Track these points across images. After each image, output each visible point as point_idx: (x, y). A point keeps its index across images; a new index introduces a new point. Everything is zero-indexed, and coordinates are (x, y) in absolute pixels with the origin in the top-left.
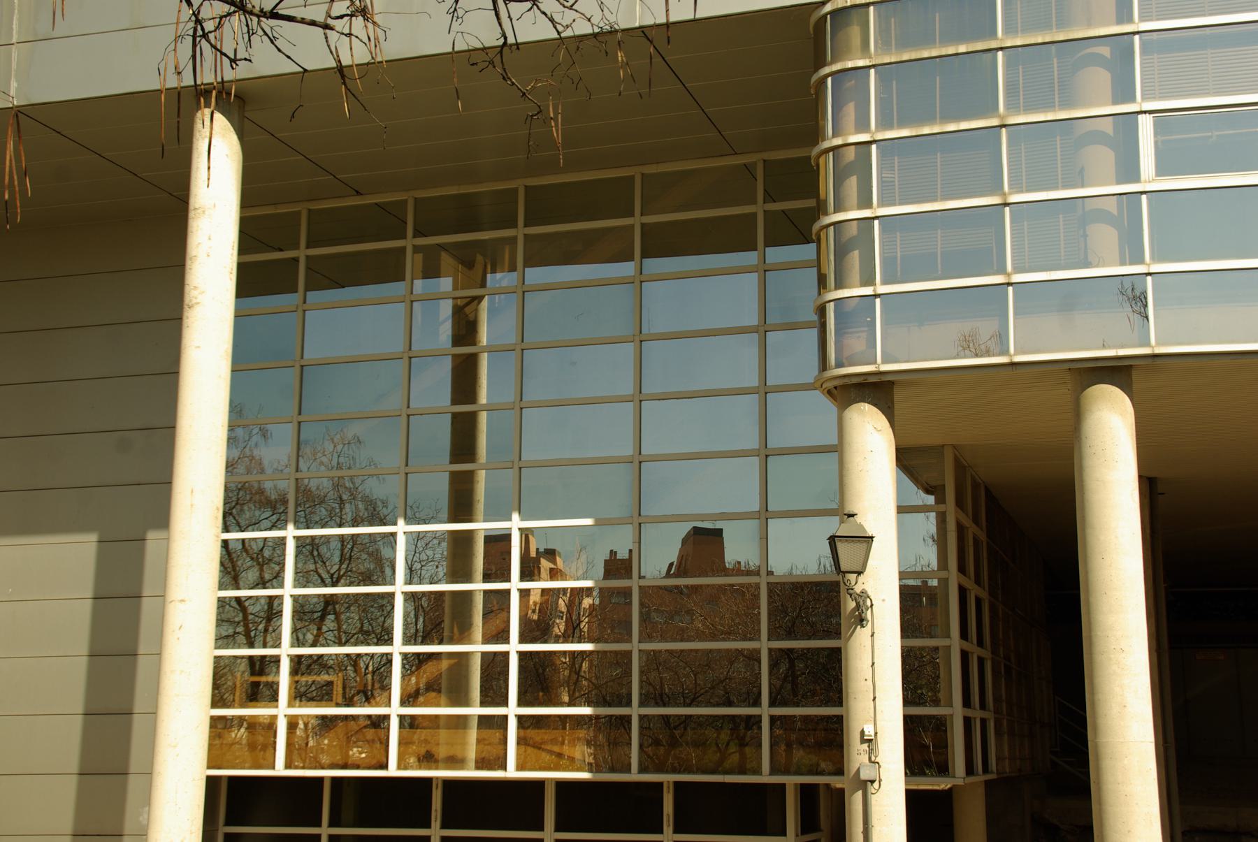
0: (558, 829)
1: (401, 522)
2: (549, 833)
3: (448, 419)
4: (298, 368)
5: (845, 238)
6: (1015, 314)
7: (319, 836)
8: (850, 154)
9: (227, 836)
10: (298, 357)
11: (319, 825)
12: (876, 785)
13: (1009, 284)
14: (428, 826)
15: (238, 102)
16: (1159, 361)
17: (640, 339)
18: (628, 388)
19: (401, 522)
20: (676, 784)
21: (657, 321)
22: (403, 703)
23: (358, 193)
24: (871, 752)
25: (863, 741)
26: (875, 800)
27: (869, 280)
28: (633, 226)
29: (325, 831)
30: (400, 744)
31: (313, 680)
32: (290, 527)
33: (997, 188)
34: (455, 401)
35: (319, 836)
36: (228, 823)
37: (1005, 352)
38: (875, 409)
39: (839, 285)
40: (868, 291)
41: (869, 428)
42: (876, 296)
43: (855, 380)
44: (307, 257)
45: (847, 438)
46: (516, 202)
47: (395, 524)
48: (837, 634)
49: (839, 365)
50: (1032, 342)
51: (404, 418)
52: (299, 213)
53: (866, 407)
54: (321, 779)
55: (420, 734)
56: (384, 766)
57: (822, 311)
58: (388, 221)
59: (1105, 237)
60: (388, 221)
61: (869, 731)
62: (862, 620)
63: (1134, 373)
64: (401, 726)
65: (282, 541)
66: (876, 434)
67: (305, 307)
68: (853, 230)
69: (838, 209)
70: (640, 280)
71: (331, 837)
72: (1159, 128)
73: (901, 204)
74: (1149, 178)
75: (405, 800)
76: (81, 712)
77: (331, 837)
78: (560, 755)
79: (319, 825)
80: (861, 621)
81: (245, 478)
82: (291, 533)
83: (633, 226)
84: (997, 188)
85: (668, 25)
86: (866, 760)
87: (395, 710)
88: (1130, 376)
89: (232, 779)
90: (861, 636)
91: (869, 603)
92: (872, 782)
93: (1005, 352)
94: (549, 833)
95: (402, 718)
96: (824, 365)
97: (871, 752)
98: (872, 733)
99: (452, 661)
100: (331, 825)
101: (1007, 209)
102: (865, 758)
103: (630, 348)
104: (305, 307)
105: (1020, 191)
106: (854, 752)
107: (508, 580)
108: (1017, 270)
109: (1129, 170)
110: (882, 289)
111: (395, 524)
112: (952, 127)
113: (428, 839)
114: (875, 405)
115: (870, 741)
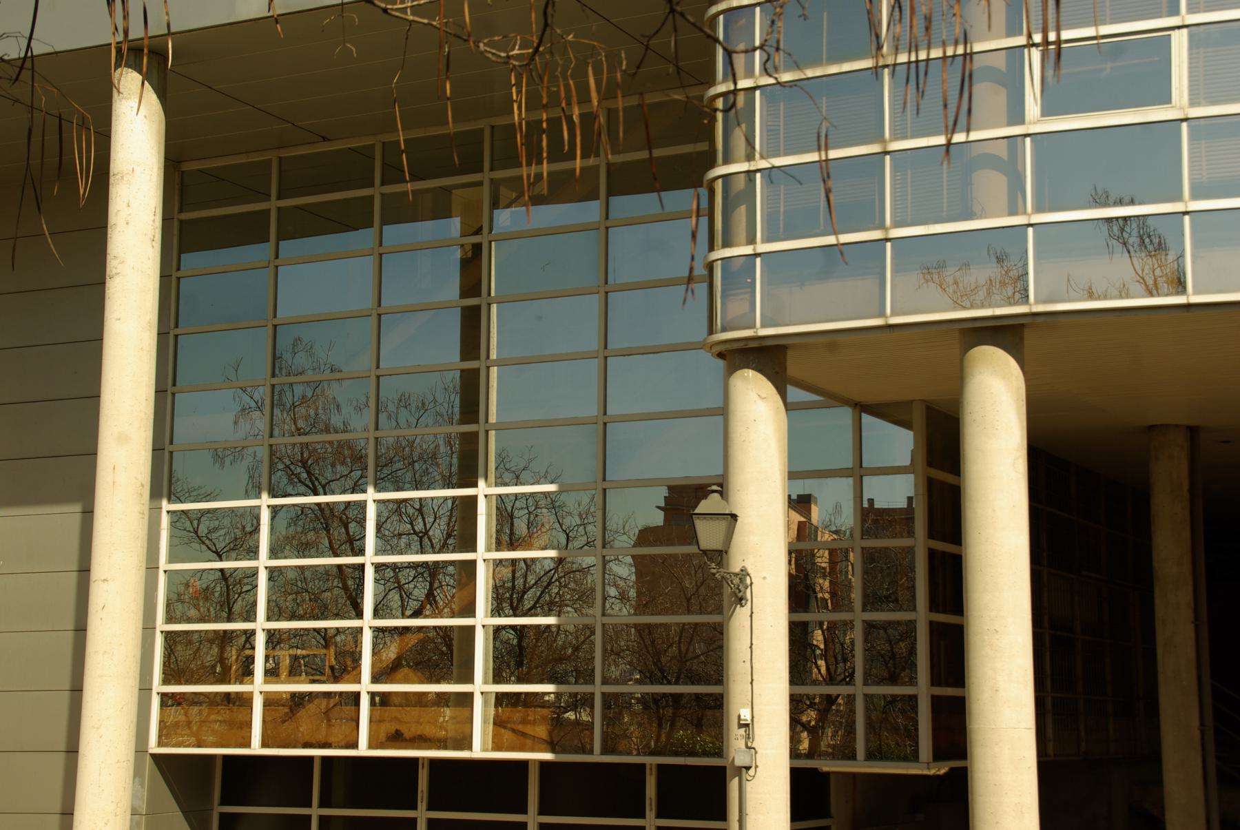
0: (541, 813)
1: (371, 490)
2: (651, 820)
3: (458, 374)
4: (270, 328)
5: (733, 193)
6: (894, 272)
7: (413, 821)
8: (741, 99)
9: (223, 816)
10: (271, 314)
11: (309, 805)
12: (752, 772)
13: (887, 240)
14: (415, 808)
15: (149, 57)
16: (1040, 320)
17: (605, 289)
18: (594, 344)
19: (371, 490)
20: (660, 767)
21: (622, 272)
22: (375, 679)
23: (324, 139)
24: (748, 737)
25: (741, 726)
26: (750, 787)
27: (751, 240)
28: (269, 211)
29: (315, 812)
30: (371, 721)
31: (294, 655)
32: (265, 496)
33: (879, 137)
34: (463, 359)
35: (413, 821)
36: (224, 802)
37: (882, 314)
38: (759, 376)
39: (727, 244)
40: (748, 250)
41: (753, 395)
42: (756, 255)
43: (736, 346)
44: (279, 208)
45: (732, 406)
46: (482, 142)
47: (365, 491)
48: (719, 610)
49: (724, 330)
50: (908, 304)
51: (373, 379)
52: (270, 160)
53: (750, 374)
54: (311, 758)
55: (392, 711)
56: (354, 745)
57: (710, 266)
58: (353, 168)
59: (991, 183)
60: (353, 168)
61: (745, 714)
62: (741, 599)
63: (790, 354)
64: (373, 703)
65: (362, 506)
66: (759, 402)
67: (277, 262)
68: (741, 183)
69: (727, 161)
70: (606, 226)
71: (431, 822)
72: (1193, 44)
73: (786, 154)
74: (1035, 120)
75: (285, 778)
76: (68, 688)
77: (431, 822)
78: (524, 735)
79: (309, 805)
80: (740, 600)
81: (409, 432)
82: (371, 496)
83: (269, 211)
84: (879, 137)
85: (28, 62)
86: (743, 746)
87: (365, 686)
88: (1022, 339)
89: (225, 757)
90: (741, 615)
91: (748, 582)
92: (748, 768)
93: (882, 314)
94: (651, 820)
95: (373, 695)
96: (711, 331)
97: (748, 737)
98: (749, 718)
99: (421, 635)
100: (322, 804)
101: (888, 158)
102: (741, 744)
103: (594, 301)
104: (608, 223)
105: (904, 137)
106: (732, 736)
107: (474, 550)
108: (898, 224)
109: (1017, 115)
110: (762, 248)
111: (365, 491)
112: (834, 69)
113: (525, 825)
114: (760, 371)
115: (747, 725)
